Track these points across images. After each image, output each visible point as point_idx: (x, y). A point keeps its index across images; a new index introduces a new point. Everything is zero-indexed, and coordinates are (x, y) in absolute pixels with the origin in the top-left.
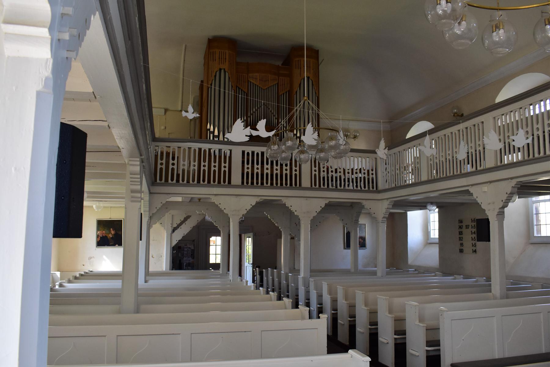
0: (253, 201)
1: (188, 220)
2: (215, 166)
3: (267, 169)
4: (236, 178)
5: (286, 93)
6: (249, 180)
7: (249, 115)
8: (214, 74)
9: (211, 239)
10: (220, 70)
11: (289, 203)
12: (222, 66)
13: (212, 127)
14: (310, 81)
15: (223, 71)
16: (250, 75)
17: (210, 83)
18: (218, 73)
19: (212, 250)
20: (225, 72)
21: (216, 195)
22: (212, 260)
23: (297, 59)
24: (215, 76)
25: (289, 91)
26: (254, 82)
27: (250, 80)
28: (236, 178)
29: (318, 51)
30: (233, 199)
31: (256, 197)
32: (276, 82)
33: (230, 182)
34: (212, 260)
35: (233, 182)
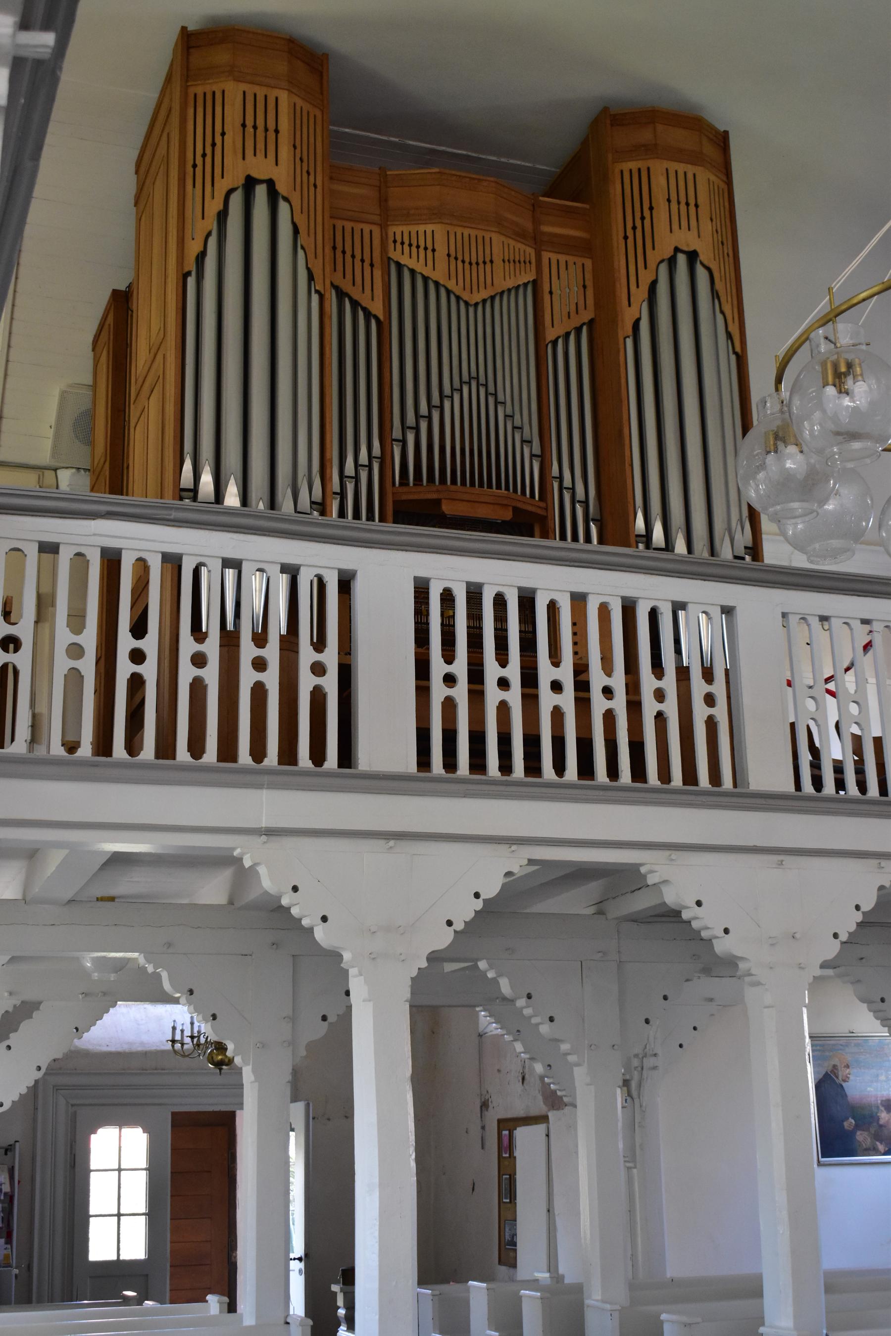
0: (490, 872)
1: (25, 1026)
2: (260, 665)
3: (556, 686)
4: (386, 734)
5: (578, 330)
6: (450, 751)
7: (397, 433)
8: (214, 206)
9: (139, 1131)
10: (250, 183)
11: (680, 883)
12: (261, 168)
13: (207, 479)
14: (702, 274)
15: (261, 191)
16: (397, 230)
17: (194, 248)
18: (237, 200)
19: (101, 1195)
20: (273, 196)
21: (270, 833)
22: (101, 1247)
23: (633, 165)
24: (222, 216)
25: (591, 323)
26: (419, 268)
27: (395, 255)
28: (386, 734)
29: (726, 133)
30: (371, 855)
31: (503, 849)
32: (530, 277)
33: (346, 757)
34: (101, 1247)
35: (370, 754)
